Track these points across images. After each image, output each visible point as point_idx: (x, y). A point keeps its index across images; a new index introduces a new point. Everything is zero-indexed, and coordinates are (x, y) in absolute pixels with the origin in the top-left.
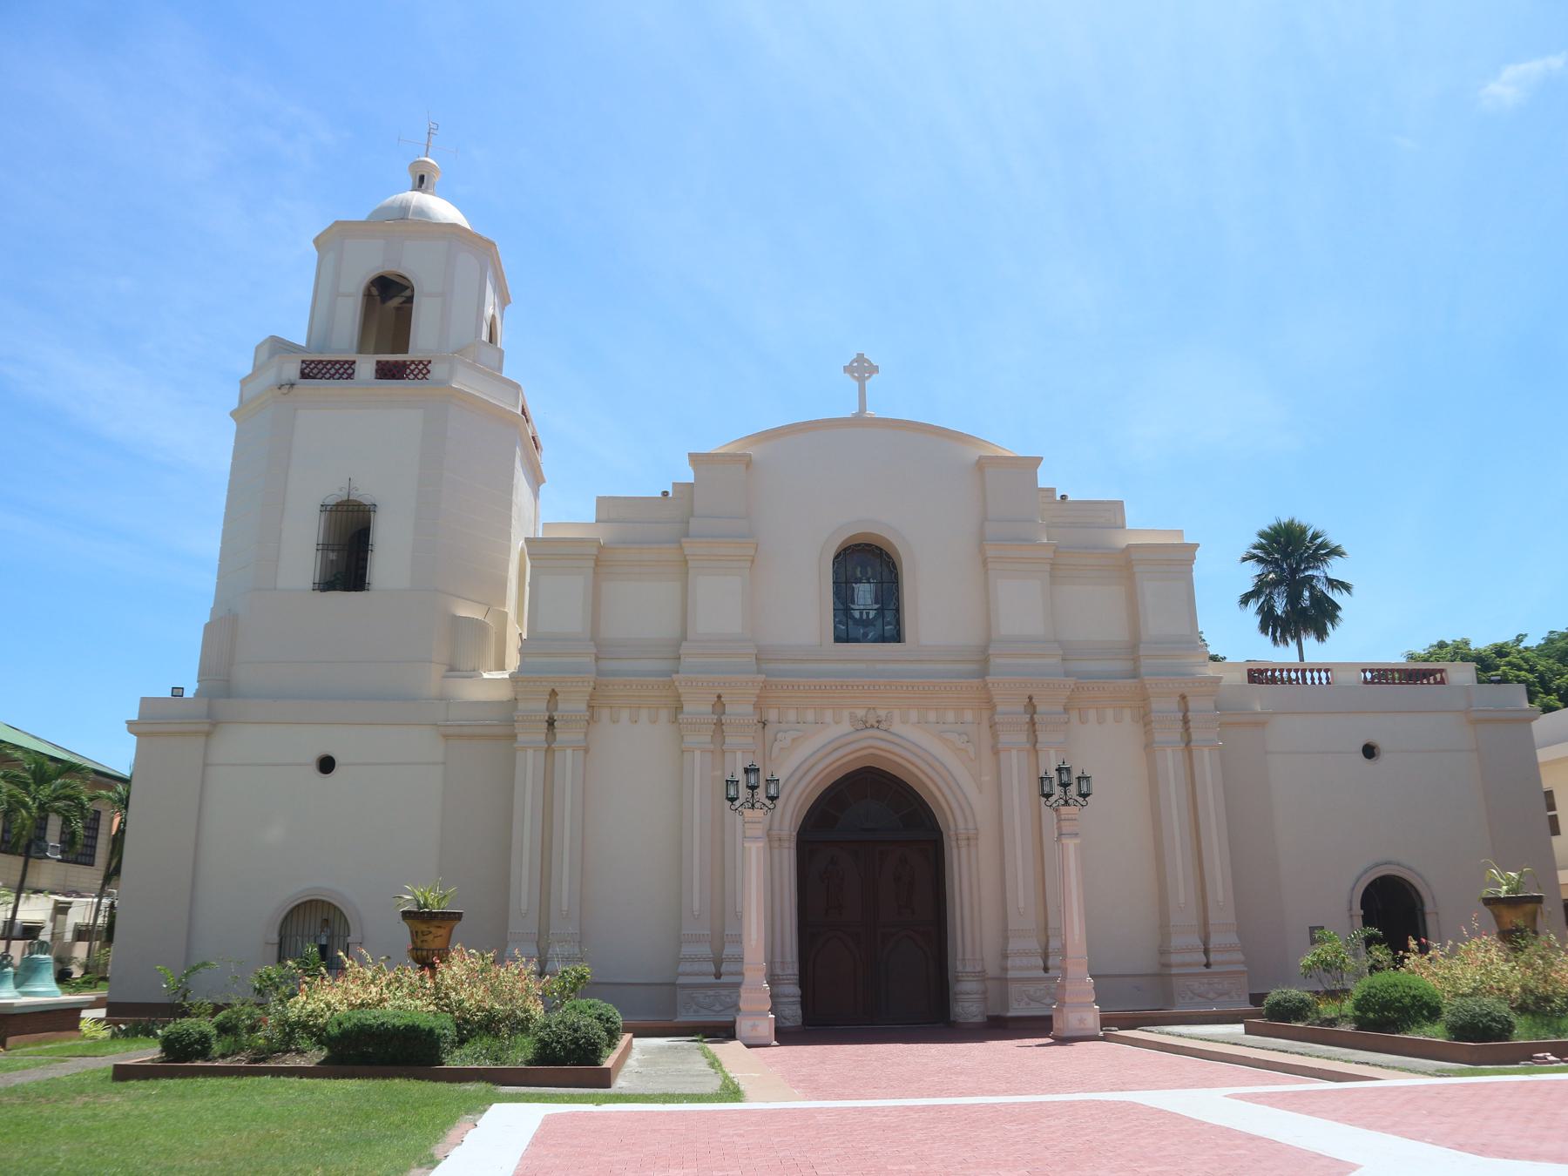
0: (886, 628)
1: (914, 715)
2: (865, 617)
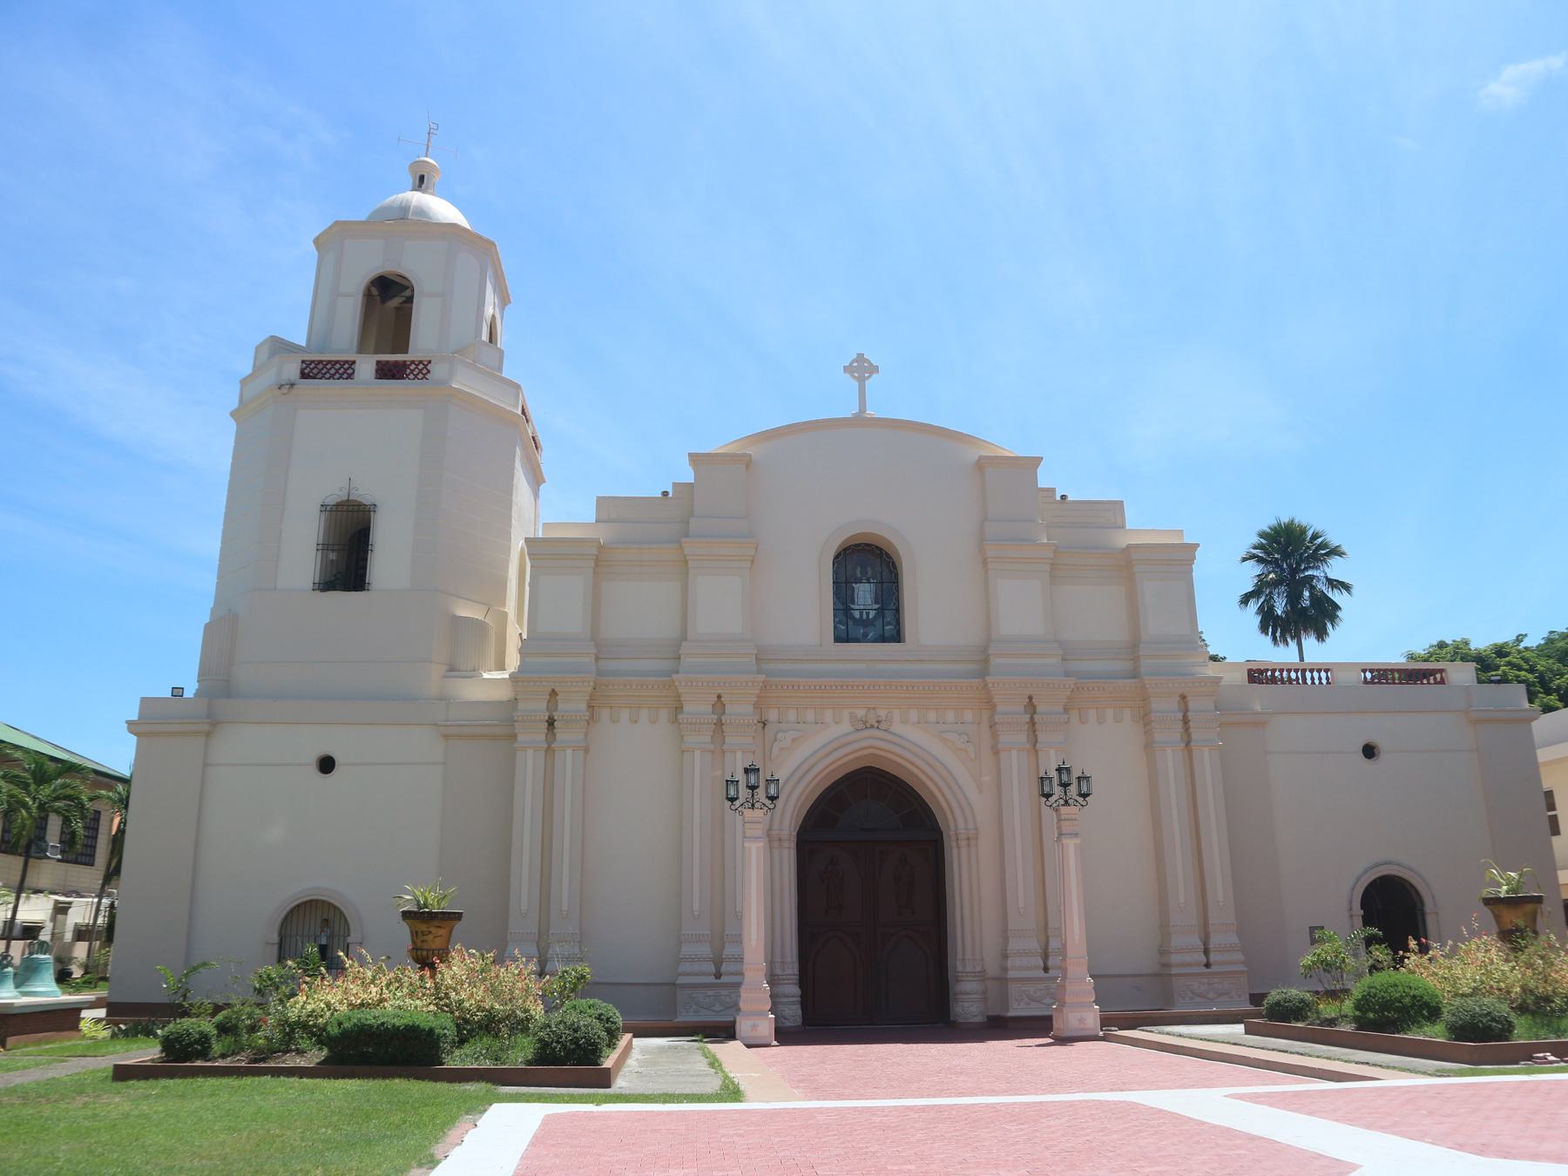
0: (886, 628)
1: (914, 715)
2: (865, 617)
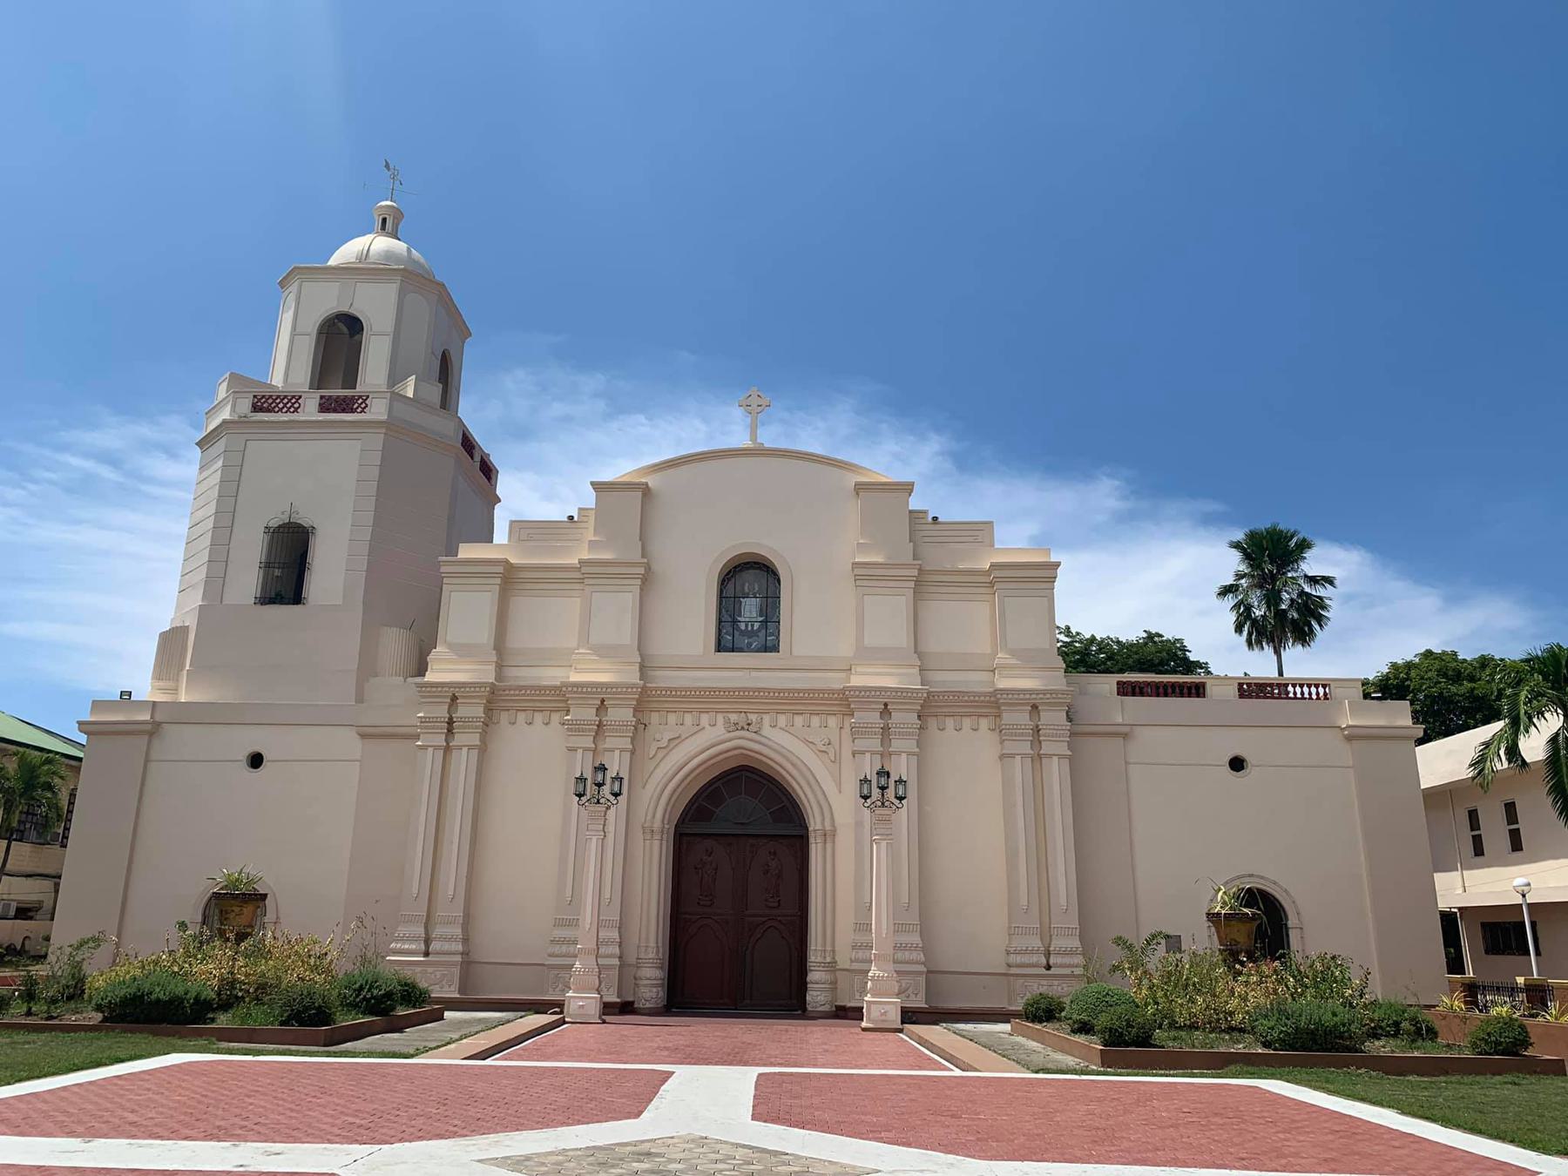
0: (768, 638)
1: (782, 720)
2: (750, 628)
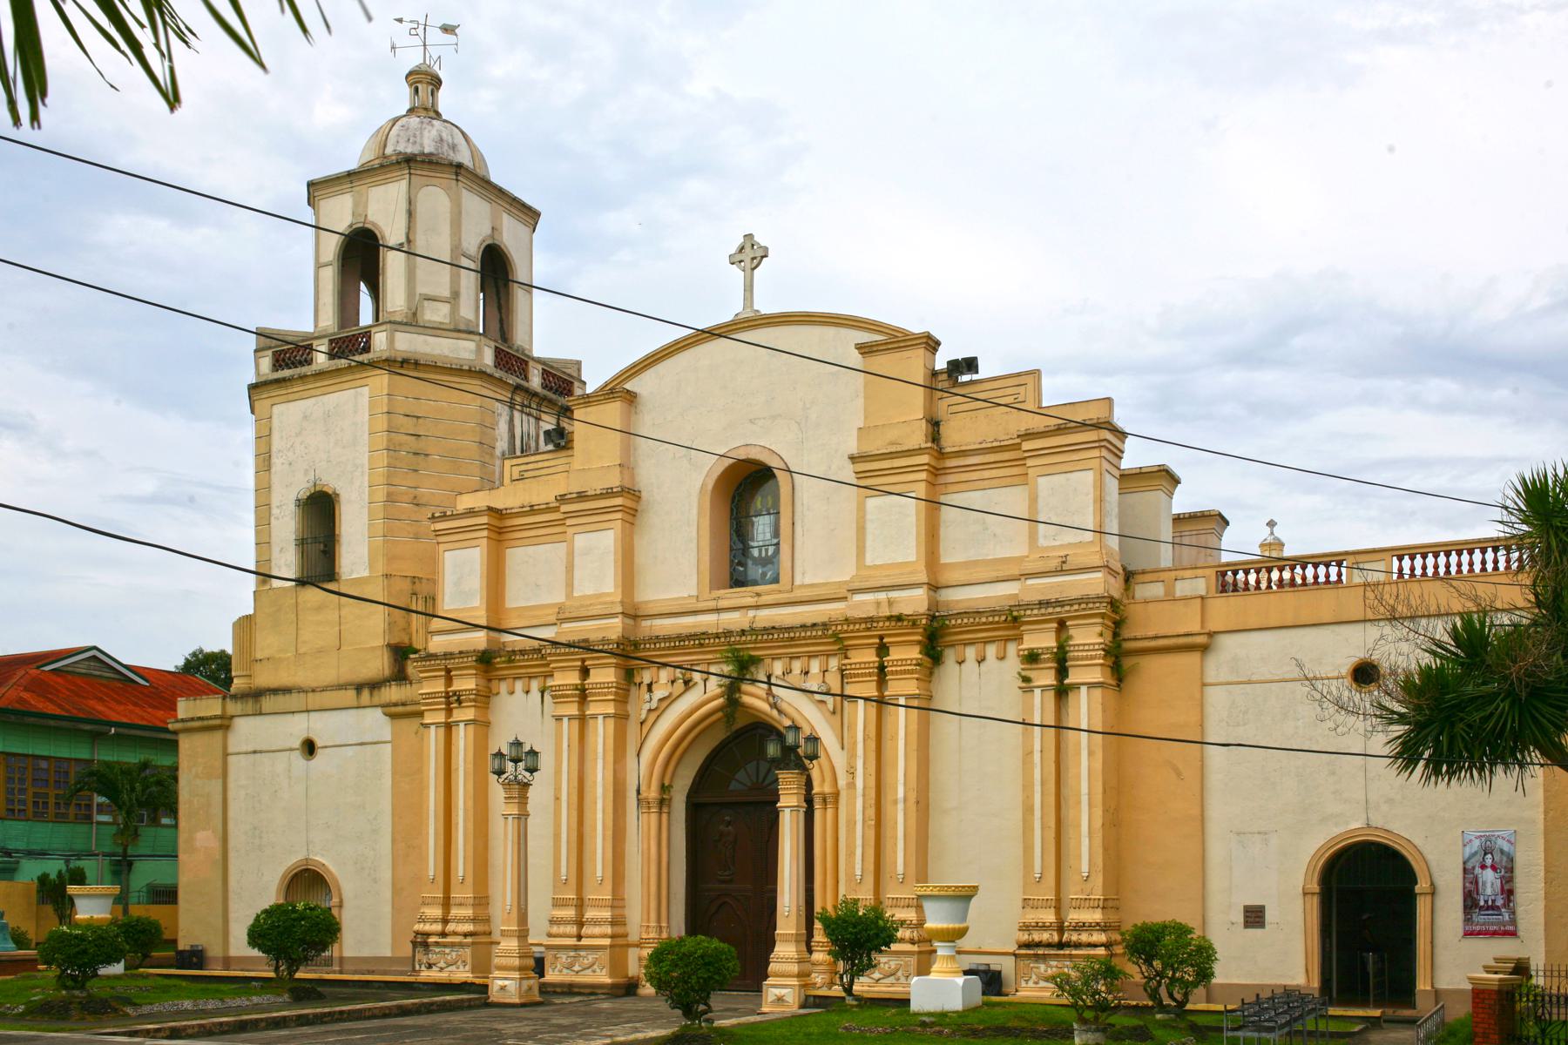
2: (763, 555)
